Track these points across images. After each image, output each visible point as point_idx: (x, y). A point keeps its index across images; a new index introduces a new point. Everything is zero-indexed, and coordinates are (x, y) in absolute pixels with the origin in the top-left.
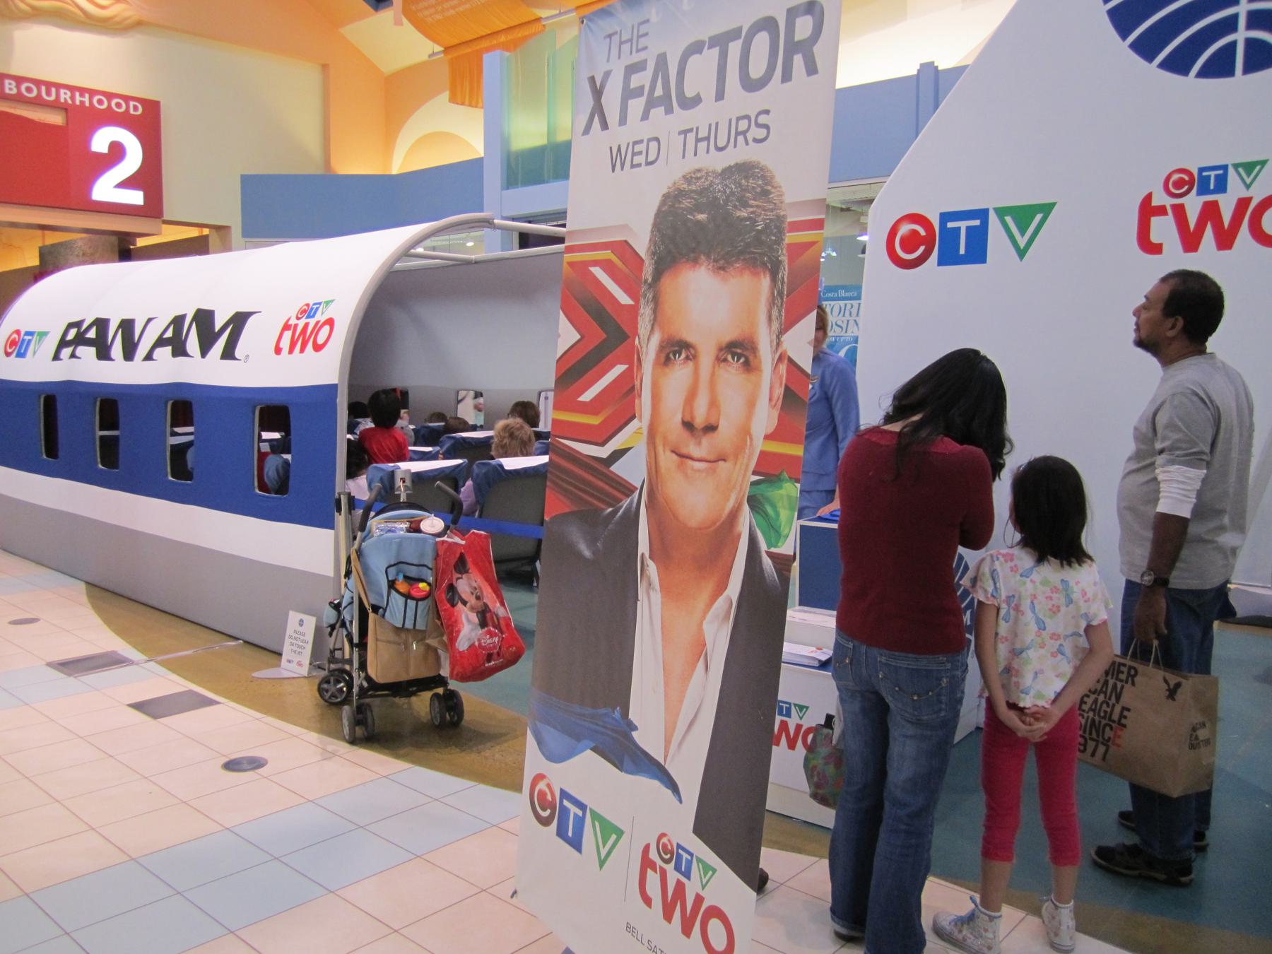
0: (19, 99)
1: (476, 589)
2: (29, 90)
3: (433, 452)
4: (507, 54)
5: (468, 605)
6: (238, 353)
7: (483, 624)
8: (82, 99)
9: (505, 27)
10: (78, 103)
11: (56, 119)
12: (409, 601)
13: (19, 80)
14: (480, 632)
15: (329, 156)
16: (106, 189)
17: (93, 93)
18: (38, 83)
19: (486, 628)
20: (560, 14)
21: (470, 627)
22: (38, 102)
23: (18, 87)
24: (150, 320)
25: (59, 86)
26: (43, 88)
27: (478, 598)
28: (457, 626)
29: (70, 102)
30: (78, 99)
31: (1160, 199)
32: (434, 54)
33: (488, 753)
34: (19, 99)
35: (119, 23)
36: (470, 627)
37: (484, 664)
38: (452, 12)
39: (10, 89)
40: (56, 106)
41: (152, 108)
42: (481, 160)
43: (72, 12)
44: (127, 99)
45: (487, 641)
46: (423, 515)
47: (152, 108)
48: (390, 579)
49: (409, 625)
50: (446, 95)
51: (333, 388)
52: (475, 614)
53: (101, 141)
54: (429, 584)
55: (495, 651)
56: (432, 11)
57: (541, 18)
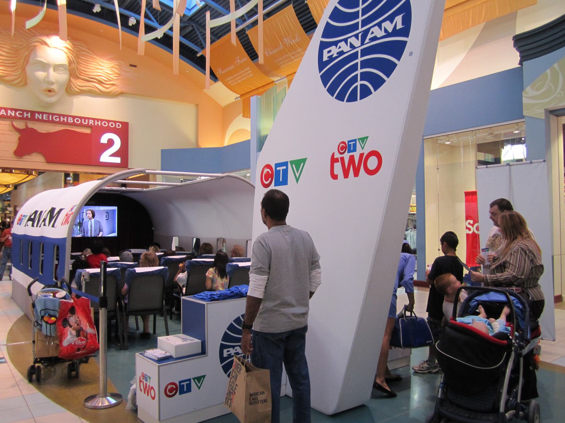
0: (74, 124)
1: (77, 321)
2: (77, 121)
3: (134, 265)
4: (259, 96)
5: (72, 327)
6: (55, 226)
7: (78, 335)
8: (98, 123)
9: (261, 85)
10: (96, 125)
11: (88, 131)
12: (47, 324)
13: (74, 117)
14: (76, 339)
15: (198, 140)
16: (105, 157)
17: (102, 120)
18: (81, 118)
19: (79, 337)
20: (281, 79)
21: (71, 336)
22: (81, 125)
23: (73, 120)
24: (46, 211)
25: (89, 119)
26: (83, 120)
27: (78, 325)
28: (64, 336)
29: (93, 124)
30: (96, 123)
31: (337, 156)
32: (237, 98)
33: (72, 390)
34: (74, 124)
35: (114, 93)
36: (71, 336)
37: (75, 352)
38: (240, 81)
39: (70, 121)
40: (87, 126)
41: (125, 125)
42: (249, 140)
43: (96, 91)
44: (115, 122)
45: (79, 342)
46: (58, 290)
47: (125, 125)
48: (42, 315)
49: (49, 334)
50: (242, 115)
51: (64, 240)
52: (75, 331)
53: (104, 139)
54: (57, 318)
55: (82, 347)
56: (233, 81)
57: (274, 81)
